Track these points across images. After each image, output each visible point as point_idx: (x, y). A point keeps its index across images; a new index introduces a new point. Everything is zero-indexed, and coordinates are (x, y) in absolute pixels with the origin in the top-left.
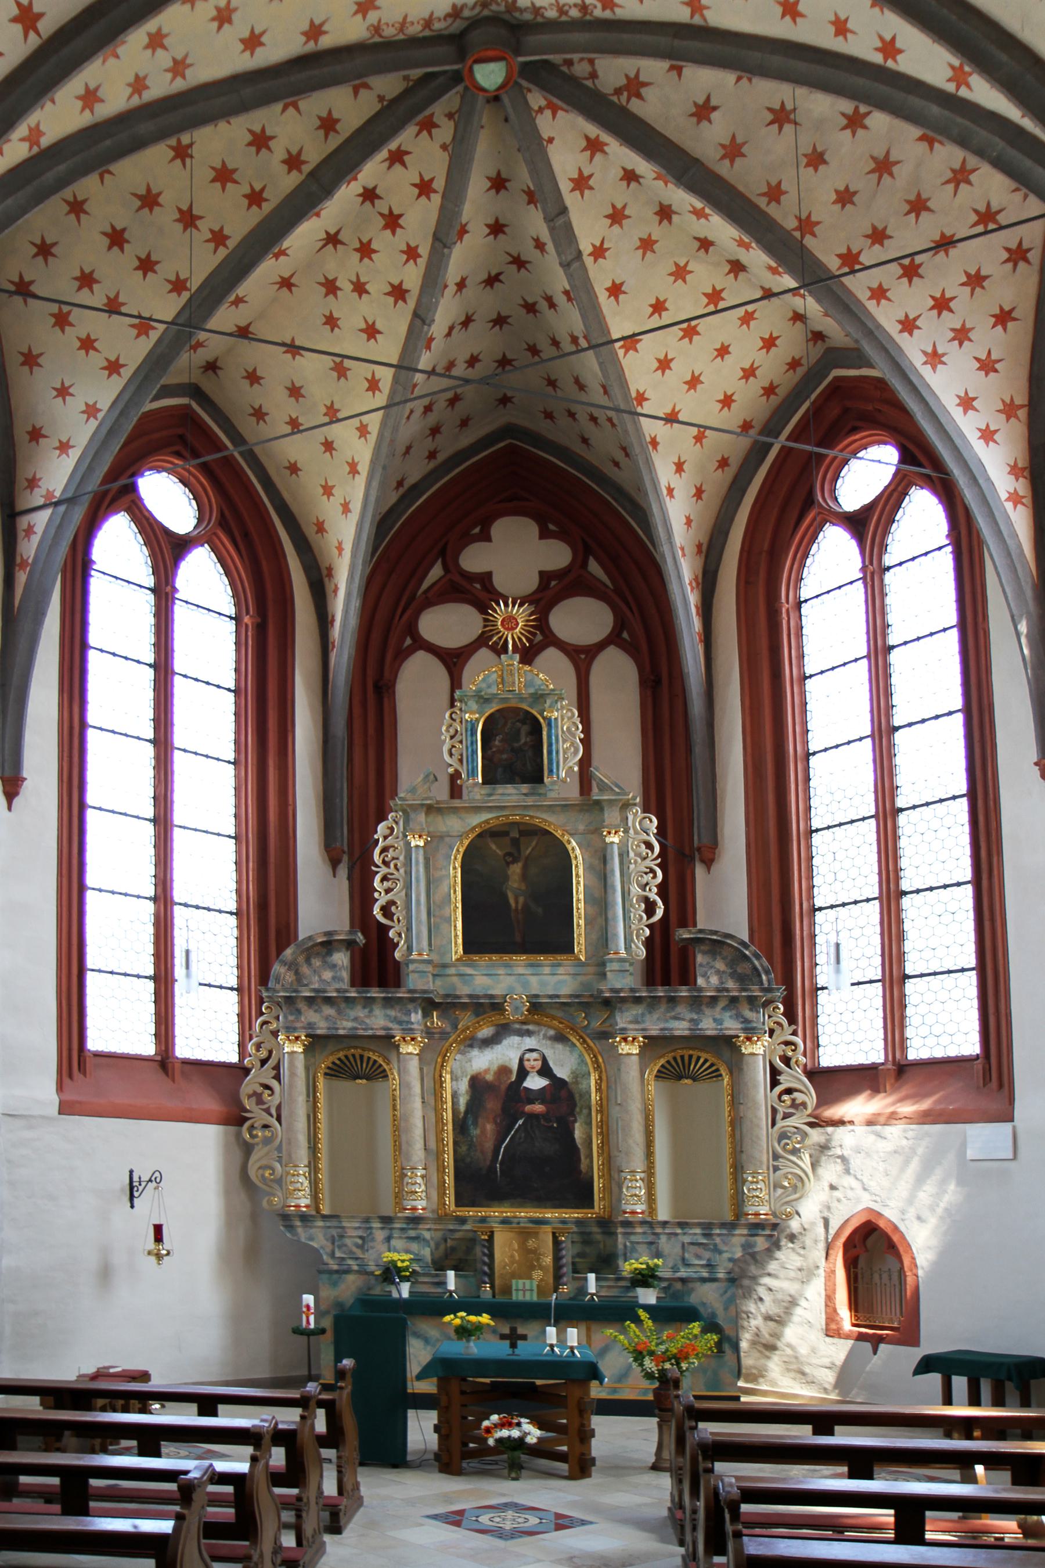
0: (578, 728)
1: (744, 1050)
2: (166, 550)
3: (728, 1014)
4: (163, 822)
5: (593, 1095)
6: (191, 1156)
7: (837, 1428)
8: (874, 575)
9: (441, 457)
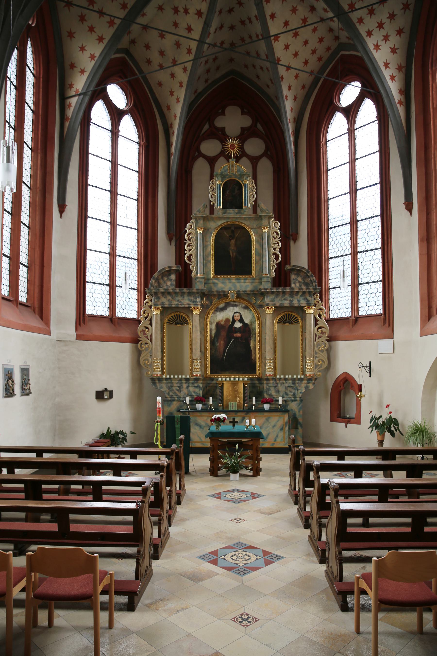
0: (254, 188)
1: (307, 312)
2: (116, 115)
3: (302, 298)
4: (113, 223)
5: (257, 329)
6: (119, 354)
7: (346, 457)
8: (351, 131)
9: (210, 82)
